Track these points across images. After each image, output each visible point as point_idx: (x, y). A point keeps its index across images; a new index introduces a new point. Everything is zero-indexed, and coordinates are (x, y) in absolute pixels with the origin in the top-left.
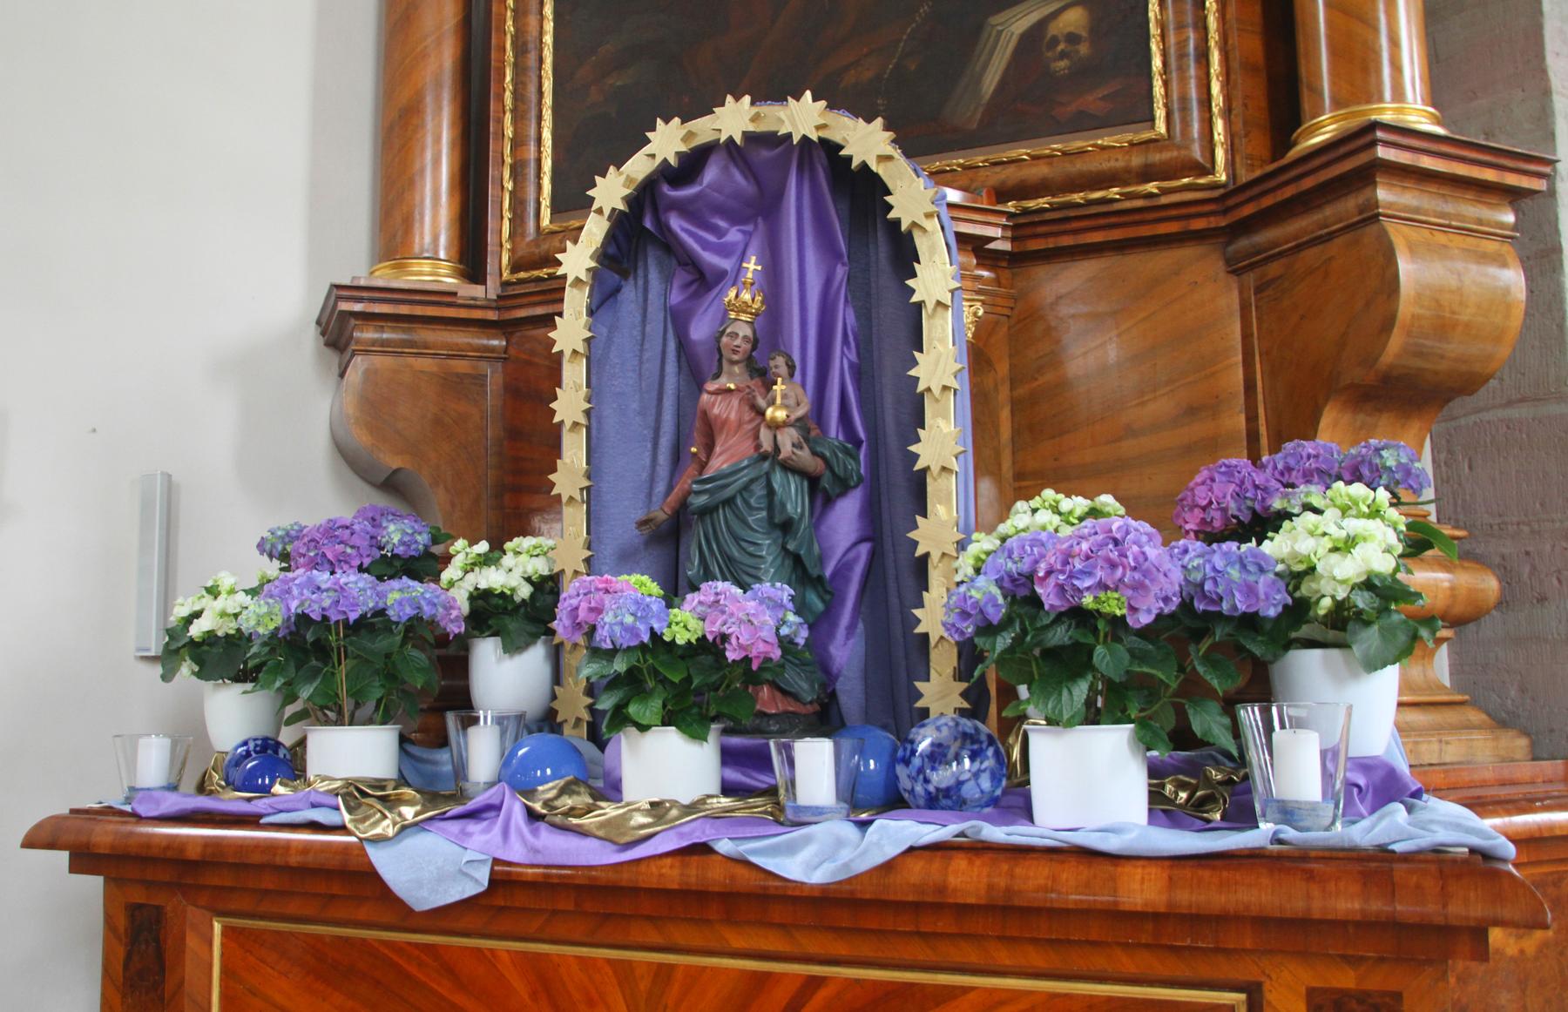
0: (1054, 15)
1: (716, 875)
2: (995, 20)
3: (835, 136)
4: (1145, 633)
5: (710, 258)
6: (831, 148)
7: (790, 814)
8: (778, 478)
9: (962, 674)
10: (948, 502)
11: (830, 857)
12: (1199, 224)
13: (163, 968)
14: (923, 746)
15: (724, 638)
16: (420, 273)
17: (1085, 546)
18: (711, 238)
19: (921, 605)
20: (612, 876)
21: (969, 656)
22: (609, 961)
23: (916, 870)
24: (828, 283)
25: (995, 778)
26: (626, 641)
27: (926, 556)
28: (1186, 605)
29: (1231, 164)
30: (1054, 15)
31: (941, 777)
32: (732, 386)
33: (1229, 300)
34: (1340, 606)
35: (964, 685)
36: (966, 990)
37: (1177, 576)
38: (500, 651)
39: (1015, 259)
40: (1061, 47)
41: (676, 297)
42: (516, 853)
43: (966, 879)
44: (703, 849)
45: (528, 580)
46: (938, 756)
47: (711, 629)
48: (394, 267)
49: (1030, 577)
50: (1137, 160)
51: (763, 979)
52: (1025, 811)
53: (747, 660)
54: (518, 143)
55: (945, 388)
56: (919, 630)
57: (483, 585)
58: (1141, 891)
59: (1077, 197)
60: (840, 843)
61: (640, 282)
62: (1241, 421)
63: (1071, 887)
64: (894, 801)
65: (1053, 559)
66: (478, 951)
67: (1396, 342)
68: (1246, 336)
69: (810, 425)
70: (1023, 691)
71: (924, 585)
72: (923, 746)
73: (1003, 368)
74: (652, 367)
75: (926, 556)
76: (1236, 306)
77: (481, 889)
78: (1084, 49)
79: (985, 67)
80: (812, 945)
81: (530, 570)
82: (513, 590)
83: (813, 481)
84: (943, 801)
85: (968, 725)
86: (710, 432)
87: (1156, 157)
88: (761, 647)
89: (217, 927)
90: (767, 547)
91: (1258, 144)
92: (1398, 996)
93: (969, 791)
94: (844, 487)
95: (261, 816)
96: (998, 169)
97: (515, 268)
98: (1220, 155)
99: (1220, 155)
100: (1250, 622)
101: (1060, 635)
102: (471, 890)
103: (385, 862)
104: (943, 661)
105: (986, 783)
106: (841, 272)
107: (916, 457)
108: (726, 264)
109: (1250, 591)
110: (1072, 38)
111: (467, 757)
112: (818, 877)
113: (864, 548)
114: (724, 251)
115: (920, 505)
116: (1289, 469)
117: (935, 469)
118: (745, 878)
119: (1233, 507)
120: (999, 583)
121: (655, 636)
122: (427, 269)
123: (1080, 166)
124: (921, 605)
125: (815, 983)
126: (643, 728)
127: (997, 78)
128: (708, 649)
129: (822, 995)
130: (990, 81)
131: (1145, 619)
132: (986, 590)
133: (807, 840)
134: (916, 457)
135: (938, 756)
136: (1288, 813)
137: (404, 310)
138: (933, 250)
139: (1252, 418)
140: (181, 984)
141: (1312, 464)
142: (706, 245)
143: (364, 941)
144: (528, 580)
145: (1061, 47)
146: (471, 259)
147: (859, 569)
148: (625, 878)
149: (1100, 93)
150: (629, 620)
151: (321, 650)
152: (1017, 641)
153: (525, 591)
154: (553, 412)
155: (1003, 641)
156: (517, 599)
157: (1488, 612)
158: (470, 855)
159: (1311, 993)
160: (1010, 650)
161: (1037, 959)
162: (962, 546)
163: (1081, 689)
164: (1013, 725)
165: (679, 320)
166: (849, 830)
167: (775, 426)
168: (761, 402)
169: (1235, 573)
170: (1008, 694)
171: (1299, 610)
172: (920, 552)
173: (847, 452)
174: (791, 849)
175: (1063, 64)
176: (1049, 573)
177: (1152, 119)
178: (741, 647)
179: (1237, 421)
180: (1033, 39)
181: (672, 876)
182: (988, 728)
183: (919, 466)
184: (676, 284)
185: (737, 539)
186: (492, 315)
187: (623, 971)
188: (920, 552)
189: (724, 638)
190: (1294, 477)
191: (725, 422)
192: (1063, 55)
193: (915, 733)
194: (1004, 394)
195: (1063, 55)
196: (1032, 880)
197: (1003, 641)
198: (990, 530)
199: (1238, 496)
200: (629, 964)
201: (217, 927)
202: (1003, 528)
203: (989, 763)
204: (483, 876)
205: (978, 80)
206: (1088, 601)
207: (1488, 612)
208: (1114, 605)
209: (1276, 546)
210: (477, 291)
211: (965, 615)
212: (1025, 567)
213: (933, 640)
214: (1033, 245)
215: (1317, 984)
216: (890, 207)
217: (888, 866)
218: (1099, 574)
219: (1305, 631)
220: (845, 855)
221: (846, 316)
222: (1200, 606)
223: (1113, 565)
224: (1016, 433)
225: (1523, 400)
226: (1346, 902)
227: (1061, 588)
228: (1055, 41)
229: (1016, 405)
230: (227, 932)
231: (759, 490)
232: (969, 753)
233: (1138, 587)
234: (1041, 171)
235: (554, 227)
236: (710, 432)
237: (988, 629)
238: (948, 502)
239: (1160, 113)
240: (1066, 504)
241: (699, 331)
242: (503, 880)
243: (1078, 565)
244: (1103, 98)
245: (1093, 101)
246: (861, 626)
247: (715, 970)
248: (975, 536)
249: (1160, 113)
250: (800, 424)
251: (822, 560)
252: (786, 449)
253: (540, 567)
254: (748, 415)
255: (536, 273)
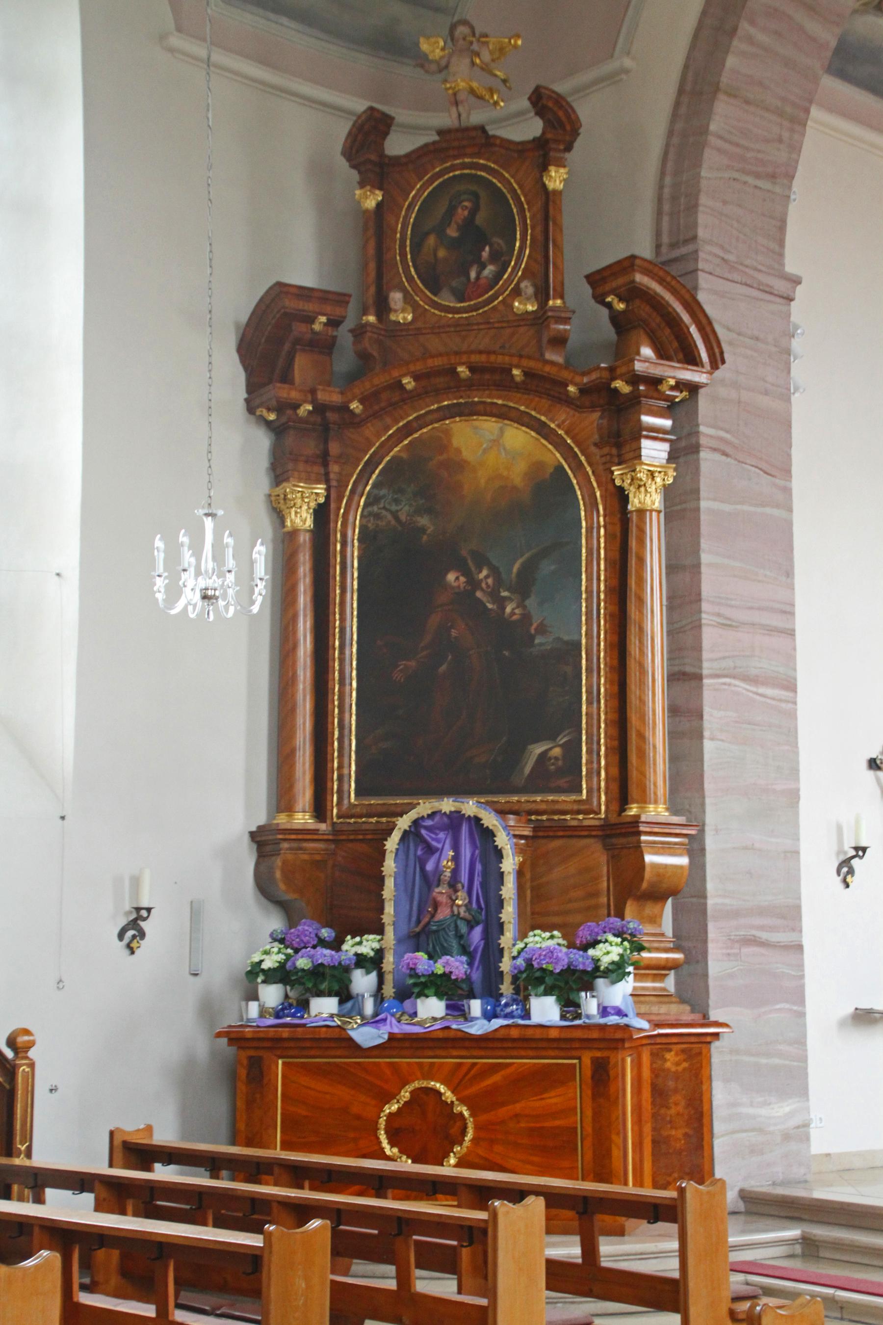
0: (551, 749)
1: (451, 1034)
2: (530, 747)
3: (480, 816)
4: (559, 974)
5: (434, 843)
6: (477, 820)
7: (469, 1019)
8: (459, 922)
9: (513, 983)
10: (510, 931)
11: (482, 1028)
12: (594, 833)
13: (263, 1077)
14: (503, 1002)
15: (451, 972)
16: (298, 819)
17: (544, 953)
18: (433, 836)
19: (501, 962)
20: (424, 1036)
21: (515, 979)
22: (416, 1063)
23: (503, 1032)
24: (473, 855)
25: (522, 1011)
26: (425, 973)
27: (503, 948)
28: (569, 967)
29: (606, 811)
30: (551, 749)
31: (509, 1010)
32: (444, 891)
33: (603, 859)
34: (607, 968)
35: (513, 986)
36: (514, 1063)
37: (566, 960)
38: (362, 974)
39: (534, 837)
40: (552, 761)
41: (419, 853)
42: (396, 1030)
43: (515, 1033)
44: (448, 1028)
45: (373, 949)
46: (507, 1005)
47: (447, 970)
48: (287, 816)
49: (531, 959)
50: (576, 807)
51: (460, 1064)
52: (529, 1018)
53: (457, 979)
54: (340, 767)
55: (510, 898)
56: (501, 970)
57: (359, 952)
58: (554, 1034)
59: (556, 817)
60: (484, 1025)
61: (406, 845)
62: (605, 900)
63: (538, 1034)
64: (496, 1016)
65: (536, 956)
66: (374, 1063)
67: (645, 885)
68: (608, 871)
69: (468, 906)
70: (530, 987)
71: (502, 957)
72: (503, 1002)
73: (528, 876)
74: (411, 870)
75: (503, 948)
76: (605, 861)
77: (384, 1041)
78: (560, 763)
79: (526, 763)
80: (475, 1053)
81: (373, 947)
82: (368, 953)
83: (468, 922)
84: (507, 1016)
85: (515, 996)
86: (436, 905)
87: (583, 807)
88: (461, 975)
89: (280, 1062)
90: (454, 943)
91: (615, 807)
92: (608, 1058)
93: (515, 1013)
94: (478, 923)
95: (306, 1024)
96: (529, 804)
97: (339, 817)
98: (603, 808)
99: (603, 808)
100: (584, 972)
101: (538, 974)
102: (381, 1041)
103: (353, 1034)
104: (507, 979)
105: (519, 1011)
106: (477, 852)
107: (501, 918)
108: (440, 846)
109: (584, 964)
110: (556, 758)
111: (363, 1006)
112: (479, 1033)
113: (482, 942)
114: (438, 841)
115: (502, 932)
116: (605, 927)
117: (506, 922)
118: (460, 1034)
119: (589, 938)
120: (524, 960)
121: (433, 972)
122: (300, 817)
123: (557, 807)
124: (501, 962)
125: (475, 1064)
126: (427, 996)
127: (530, 768)
128: (446, 976)
129: (478, 1066)
130: (527, 770)
131: (558, 971)
132: (520, 962)
133: (476, 1024)
134: (501, 918)
135: (507, 1005)
136: (588, 1017)
137: (300, 837)
138: (508, 856)
139: (609, 899)
140: (270, 1080)
141: (611, 926)
142: (433, 839)
143: (335, 1063)
144: (373, 949)
145: (552, 761)
146: (320, 810)
147: (481, 947)
148: (427, 1036)
149: (565, 780)
150: (426, 967)
151: (323, 975)
152: (528, 976)
153: (372, 954)
154: (382, 895)
155: (524, 975)
156: (369, 956)
157: (682, 965)
158: (381, 1032)
159: (591, 1058)
160: (526, 977)
161: (531, 1053)
162: (514, 945)
163: (542, 988)
164: (527, 998)
165: (423, 864)
166: (485, 1022)
167: (459, 906)
168: (454, 898)
169: (581, 959)
170: (526, 989)
171: (597, 968)
172: (501, 946)
173: (479, 913)
174: (471, 1027)
175: (553, 767)
176: (536, 959)
177: (581, 792)
178: (456, 975)
179: (604, 900)
180: (544, 755)
181: (441, 1035)
182: (521, 998)
183: (502, 921)
184: (420, 848)
185: (446, 940)
186: (330, 837)
187: (420, 1065)
188: (501, 946)
189: (451, 972)
190: (607, 930)
191: (442, 903)
192: (553, 764)
193: (501, 999)
194: (528, 885)
195: (553, 764)
196: (529, 1033)
197: (524, 975)
198: (522, 940)
199: (590, 935)
200: (422, 1063)
201: (280, 1062)
202: (526, 940)
203: (520, 1007)
204: (386, 1037)
205: (523, 768)
206: (544, 966)
207: (682, 965)
208: (550, 967)
209: (591, 952)
210: (323, 827)
211: (515, 968)
212: (530, 956)
213: (505, 973)
214: (541, 834)
215: (592, 1055)
216: (495, 841)
217: (496, 1030)
218: (547, 960)
219: (598, 974)
220: (485, 1027)
221: (479, 867)
222: (572, 968)
223: (551, 958)
224: (532, 897)
225: (695, 896)
226: (595, 1035)
227: (538, 963)
228: (550, 759)
229: (533, 889)
230: (284, 1063)
231: (453, 925)
232: (298, 411)
233: (556, 963)
234: (543, 807)
235: (356, 803)
236: (436, 905)
237: (521, 972)
238: (510, 931)
239: (584, 792)
240: (543, 935)
241: (430, 866)
242: (392, 1037)
243: (542, 957)
244: (565, 782)
245: (562, 782)
246: (481, 967)
247: (447, 1063)
248: (518, 942)
249: (584, 792)
250: (466, 906)
251: (470, 946)
252: (462, 914)
253: (376, 945)
254: (449, 901)
255: (348, 820)
